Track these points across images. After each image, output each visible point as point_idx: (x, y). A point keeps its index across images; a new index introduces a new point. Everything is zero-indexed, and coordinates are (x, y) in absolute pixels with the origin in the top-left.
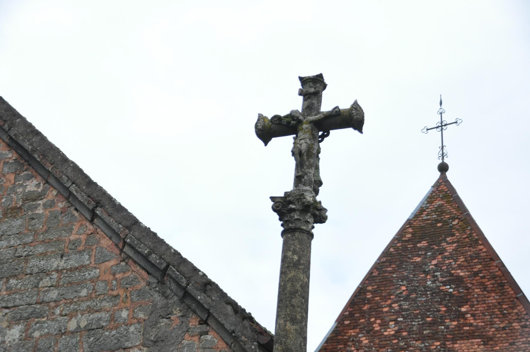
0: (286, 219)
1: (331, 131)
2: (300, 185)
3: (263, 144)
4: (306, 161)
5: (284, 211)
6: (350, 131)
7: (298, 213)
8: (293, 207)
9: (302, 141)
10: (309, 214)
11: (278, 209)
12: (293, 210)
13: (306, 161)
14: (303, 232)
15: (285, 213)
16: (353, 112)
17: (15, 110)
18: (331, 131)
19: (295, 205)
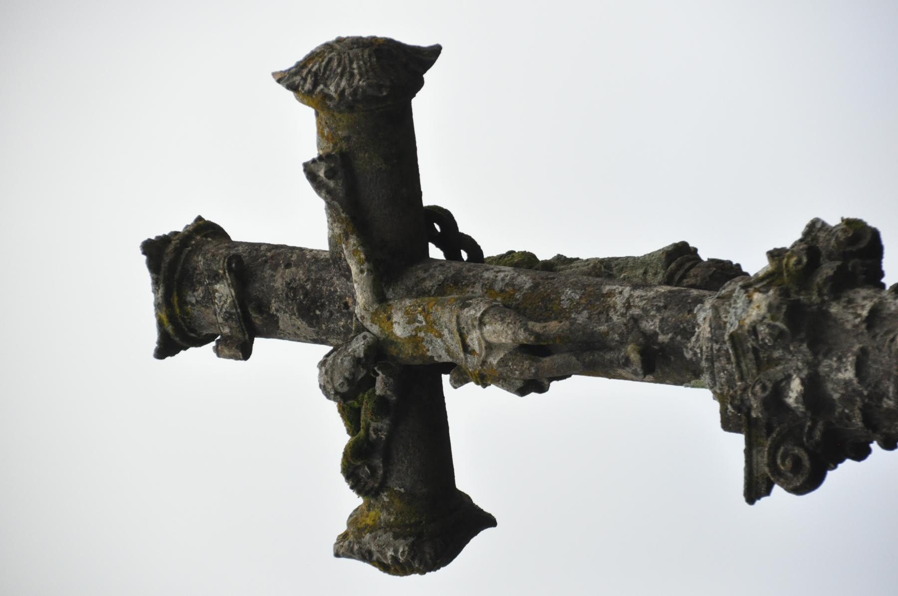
3: (485, 535)
5: (817, 435)
6: (431, 110)
7: (826, 365)
10: (835, 309)
11: (806, 462)
12: (814, 386)
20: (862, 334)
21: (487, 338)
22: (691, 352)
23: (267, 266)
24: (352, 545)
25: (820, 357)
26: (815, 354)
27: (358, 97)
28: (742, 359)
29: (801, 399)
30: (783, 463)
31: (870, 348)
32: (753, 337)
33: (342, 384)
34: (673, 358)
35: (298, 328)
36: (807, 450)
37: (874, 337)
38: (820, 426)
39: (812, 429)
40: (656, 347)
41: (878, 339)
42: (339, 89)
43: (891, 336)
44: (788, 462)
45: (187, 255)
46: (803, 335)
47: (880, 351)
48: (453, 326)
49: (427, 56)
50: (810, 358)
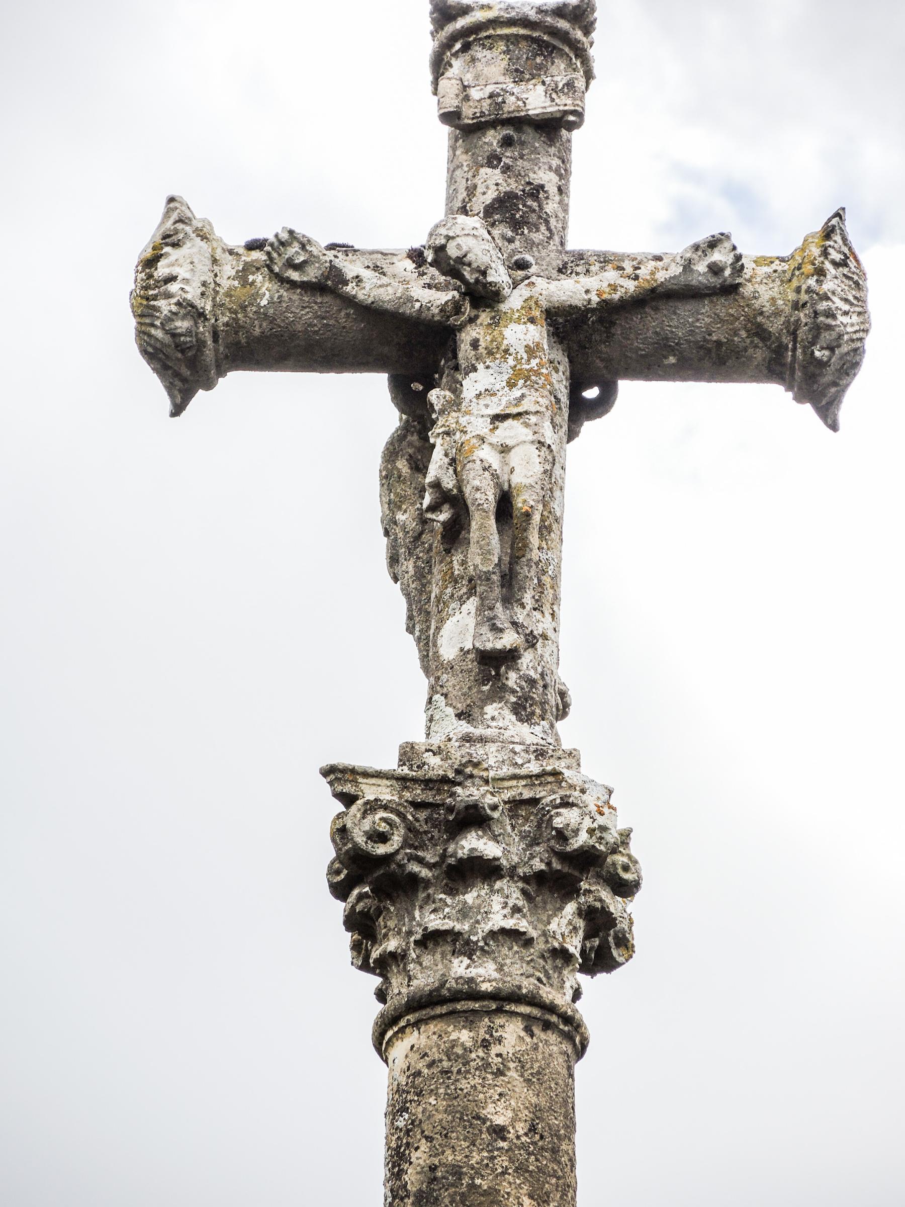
0: (435, 922)
1: (626, 387)
2: (491, 709)
3: (165, 402)
4: (465, 545)
5: (415, 868)
6: (768, 403)
7: (514, 892)
8: (489, 849)
9: (510, 431)
10: (570, 908)
11: (381, 850)
12: (484, 870)
13: (465, 545)
14: (547, 1026)
15: (427, 883)
16: (828, 285)
17: (709, 381)
18: (626, 387)
19: (495, 838)
20: (547, 942)
21: (516, 448)
22: (496, 713)
23: (559, 162)
24: (177, 228)
25: (520, 884)
26: (525, 879)
27: (821, 319)
28: (524, 783)
29: (476, 854)
30: (382, 819)
31: (532, 950)
32: (558, 801)
33: (459, 247)
34: (486, 688)
35: (484, 193)
36: (397, 852)
37: (543, 957)
38: (425, 873)
39: (421, 861)
40: (503, 669)
41: (541, 961)
42: (830, 294)
43: (544, 980)
44: (383, 827)
45: (568, 55)
46: (556, 865)
47: (528, 963)
48: (525, 406)
49: (827, 411)
50: (520, 871)
